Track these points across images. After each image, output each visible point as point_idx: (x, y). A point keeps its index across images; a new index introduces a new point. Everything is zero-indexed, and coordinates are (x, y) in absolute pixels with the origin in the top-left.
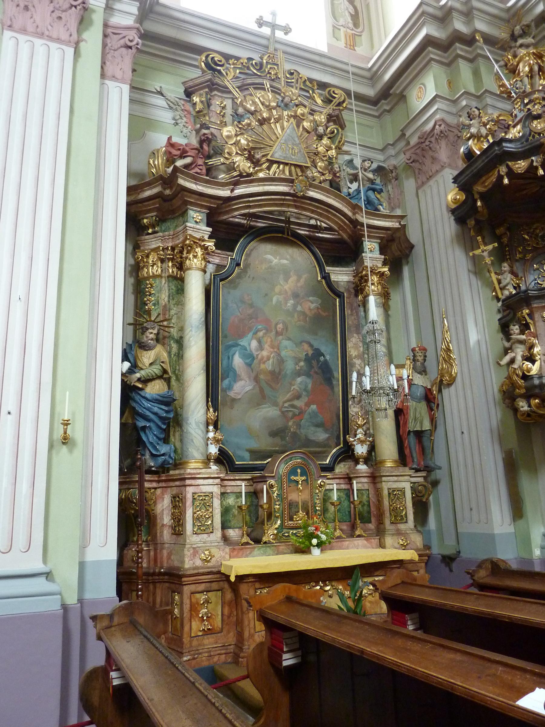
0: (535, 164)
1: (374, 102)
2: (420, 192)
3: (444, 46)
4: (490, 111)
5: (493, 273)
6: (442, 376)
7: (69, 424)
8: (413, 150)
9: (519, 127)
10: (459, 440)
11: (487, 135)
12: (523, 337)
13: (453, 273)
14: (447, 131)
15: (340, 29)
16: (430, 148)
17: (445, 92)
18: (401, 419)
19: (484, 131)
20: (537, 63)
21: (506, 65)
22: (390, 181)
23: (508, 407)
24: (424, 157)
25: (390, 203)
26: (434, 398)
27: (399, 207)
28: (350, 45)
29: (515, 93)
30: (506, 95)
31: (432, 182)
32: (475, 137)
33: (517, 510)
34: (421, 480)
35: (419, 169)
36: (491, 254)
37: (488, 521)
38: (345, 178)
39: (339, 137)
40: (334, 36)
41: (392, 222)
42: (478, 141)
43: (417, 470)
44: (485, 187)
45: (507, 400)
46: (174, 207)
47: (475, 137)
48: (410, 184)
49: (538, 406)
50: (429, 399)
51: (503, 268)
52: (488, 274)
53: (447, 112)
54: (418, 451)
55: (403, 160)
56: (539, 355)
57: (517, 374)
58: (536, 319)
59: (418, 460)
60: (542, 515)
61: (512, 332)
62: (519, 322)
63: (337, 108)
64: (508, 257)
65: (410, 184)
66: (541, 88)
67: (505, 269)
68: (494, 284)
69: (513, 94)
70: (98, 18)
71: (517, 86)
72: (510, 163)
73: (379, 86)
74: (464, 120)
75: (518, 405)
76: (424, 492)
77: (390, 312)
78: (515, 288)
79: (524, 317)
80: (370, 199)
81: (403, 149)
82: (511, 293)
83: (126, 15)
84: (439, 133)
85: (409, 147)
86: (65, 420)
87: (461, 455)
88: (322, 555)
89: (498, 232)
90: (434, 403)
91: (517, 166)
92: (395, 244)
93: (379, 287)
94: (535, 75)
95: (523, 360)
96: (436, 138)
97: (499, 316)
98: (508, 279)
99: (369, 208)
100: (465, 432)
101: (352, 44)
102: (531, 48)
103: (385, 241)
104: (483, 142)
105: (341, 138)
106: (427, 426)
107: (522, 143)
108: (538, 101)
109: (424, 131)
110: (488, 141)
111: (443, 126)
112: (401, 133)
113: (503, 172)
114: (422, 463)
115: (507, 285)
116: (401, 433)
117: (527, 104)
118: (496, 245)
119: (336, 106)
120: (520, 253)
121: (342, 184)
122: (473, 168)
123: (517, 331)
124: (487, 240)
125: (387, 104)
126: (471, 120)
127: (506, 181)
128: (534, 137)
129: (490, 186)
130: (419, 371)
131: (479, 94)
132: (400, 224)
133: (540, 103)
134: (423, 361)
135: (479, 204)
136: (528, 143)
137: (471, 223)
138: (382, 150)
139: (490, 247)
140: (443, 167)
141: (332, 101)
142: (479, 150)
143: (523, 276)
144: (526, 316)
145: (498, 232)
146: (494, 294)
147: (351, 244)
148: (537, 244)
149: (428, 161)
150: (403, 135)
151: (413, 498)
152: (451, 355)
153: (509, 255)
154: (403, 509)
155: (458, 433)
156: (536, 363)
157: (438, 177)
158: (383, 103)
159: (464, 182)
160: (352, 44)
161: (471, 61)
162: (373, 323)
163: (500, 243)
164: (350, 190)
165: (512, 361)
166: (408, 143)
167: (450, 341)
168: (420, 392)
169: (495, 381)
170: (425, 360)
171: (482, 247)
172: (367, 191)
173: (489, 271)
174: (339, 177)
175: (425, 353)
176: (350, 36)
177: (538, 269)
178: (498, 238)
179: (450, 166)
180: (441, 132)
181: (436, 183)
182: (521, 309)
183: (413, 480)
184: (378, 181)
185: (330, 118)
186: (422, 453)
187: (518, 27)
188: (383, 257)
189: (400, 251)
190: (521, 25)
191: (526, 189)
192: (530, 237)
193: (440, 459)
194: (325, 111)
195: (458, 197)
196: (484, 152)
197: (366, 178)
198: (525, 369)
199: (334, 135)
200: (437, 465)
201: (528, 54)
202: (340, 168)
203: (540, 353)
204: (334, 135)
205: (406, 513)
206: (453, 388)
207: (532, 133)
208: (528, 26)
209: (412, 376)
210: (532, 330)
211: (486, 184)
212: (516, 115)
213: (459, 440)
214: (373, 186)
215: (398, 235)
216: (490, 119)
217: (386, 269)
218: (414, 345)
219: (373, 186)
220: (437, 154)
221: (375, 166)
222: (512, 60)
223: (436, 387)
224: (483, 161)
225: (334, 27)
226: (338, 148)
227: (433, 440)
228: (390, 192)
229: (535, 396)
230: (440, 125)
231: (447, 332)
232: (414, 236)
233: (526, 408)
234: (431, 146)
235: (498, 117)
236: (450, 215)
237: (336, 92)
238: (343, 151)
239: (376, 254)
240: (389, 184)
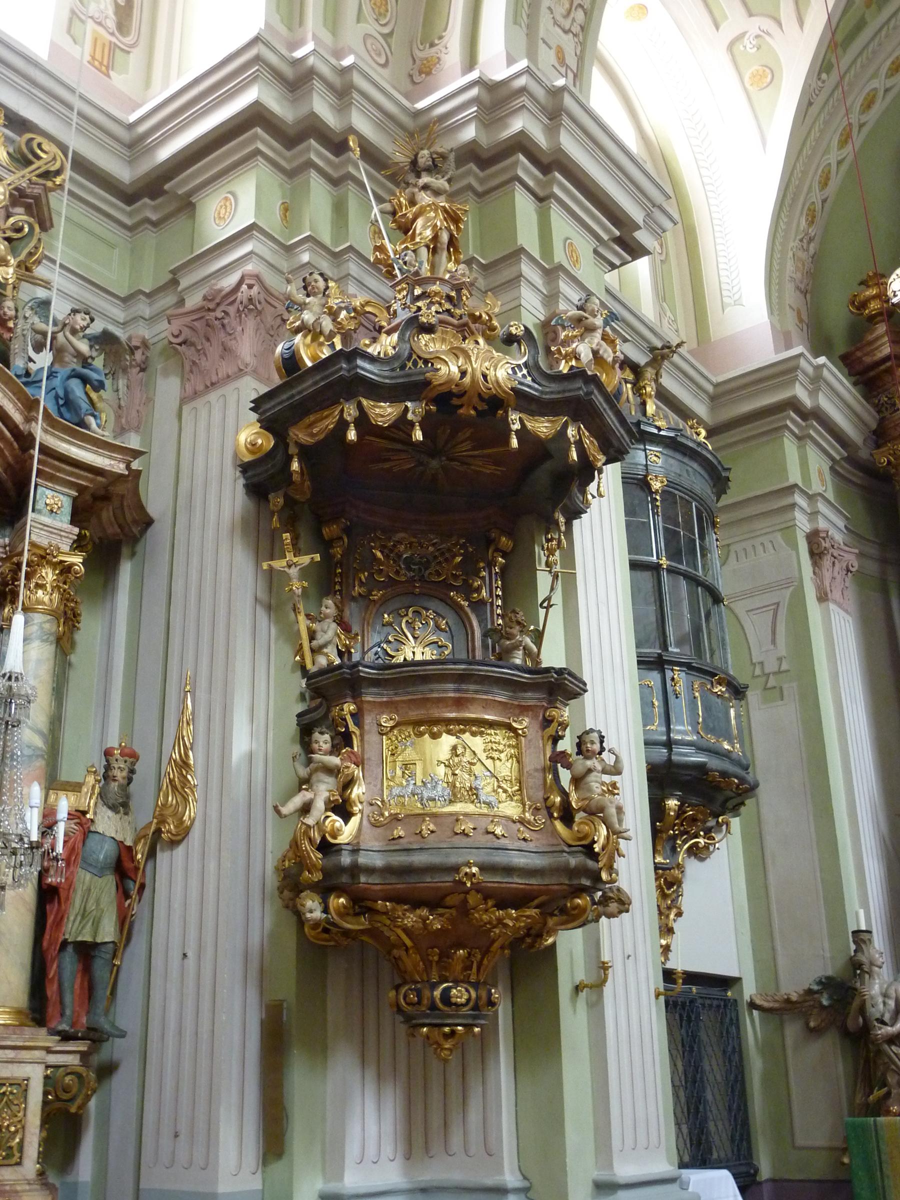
0: (410, 416)
1: (129, 196)
2: (186, 409)
3: (290, 137)
4: (352, 289)
5: (303, 614)
6: (162, 821)
8: (188, 319)
9: (395, 337)
10: (174, 974)
11: (331, 336)
12: (335, 760)
13: (222, 595)
14: (263, 301)
16: (223, 326)
17: (273, 223)
18: (52, 911)
19: (327, 324)
20: (448, 229)
21: (394, 213)
22: (125, 370)
23: (287, 907)
24: (208, 340)
25: (118, 417)
26: (137, 869)
27: (137, 429)
28: (101, 63)
29: (400, 269)
30: (384, 268)
31: (213, 396)
32: (310, 331)
33: (274, 1141)
34: (73, 1060)
35: (194, 363)
36: (305, 573)
37: (209, 1164)
38: (24, 335)
39: (32, 244)
40: (69, 31)
41: (111, 458)
42: (313, 340)
43: (66, 1037)
44: (312, 435)
45: (286, 893)
47: (310, 331)
48: (168, 388)
49: (343, 913)
50: (126, 870)
51: (323, 608)
52: (292, 615)
53: (272, 266)
54: (78, 992)
55: (163, 336)
56: (361, 803)
57: (310, 839)
58: (366, 727)
59: (73, 1012)
60: (323, 1152)
61: (315, 746)
62: (333, 726)
63: (41, 181)
64: (337, 587)
65: (168, 388)
66: (447, 276)
67: (328, 611)
68: (300, 638)
69: (397, 272)
71: (407, 258)
72: (365, 402)
73: (145, 166)
74: (295, 292)
75: (303, 905)
76: (74, 1090)
77: (73, 658)
78: (340, 654)
79: (345, 720)
80: (71, 397)
81: (169, 312)
82: (330, 663)
84: (245, 301)
85: (181, 311)
87: (173, 1007)
89: (326, 531)
90: (135, 882)
91: (378, 411)
92: (111, 508)
93: (56, 596)
94: (443, 249)
95: (326, 810)
96: (238, 310)
97: (300, 708)
98: (330, 633)
99: (67, 415)
100: (190, 954)
101: (106, 61)
102: (443, 198)
103: (87, 497)
104: (321, 344)
105: (36, 248)
106: (108, 932)
107: (393, 370)
108: (437, 299)
109: (218, 287)
110: (332, 346)
111: (256, 289)
112: (170, 276)
113: (350, 415)
114: (84, 1020)
115: (325, 645)
116: (45, 944)
117: (418, 298)
118: (317, 557)
119: (39, 176)
120: (362, 584)
121: (15, 346)
122: (294, 391)
123: (326, 747)
124: (301, 545)
125: (155, 209)
126: (308, 296)
127: (352, 435)
128: (415, 364)
129: (322, 437)
130: (111, 802)
131: (337, 250)
132: (128, 467)
133: (440, 304)
134: (125, 782)
135: (295, 466)
136: (402, 373)
137: (277, 500)
138: (126, 300)
139: (305, 560)
140: (240, 373)
141: (30, 163)
142: (313, 358)
143: (359, 632)
144: (348, 718)
145: (326, 531)
146: (298, 658)
147: (9, 485)
148: (397, 573)
149: (214, 351)
150: (174, 282)
151: (45, 1103)
152: (189, 777)
153: (341, 584)
154: (17, 1131)
155: (176, 955)
156: (353, 819)
157: (229, 390)
158: (145, 205)
159: (275, 414)
160: (106, 61)
161: (335, 182)
162: (10, 678)
163: (327, 558)
164: (31, 365)
165: (306, 809)
166: (181, 302)
167: (192, 745)
168: (104, 852)
169: (271, 847)
170: (130, 780)
171: (290, 556)
172: (70, 377)
173: (295, 609)
174: (10, 330)
175: (133, 764)
176: (104, 45)
177: (390, 624)
178: (324, 545)
179: (255, 373)
180: (250, 300)
181: (221, 400)
182: (340, 699)
183: (53, 1059)
184: (98, 363)
185: (21, 197)
186: (87, 995)
187: (425, 152)
188: (76, 530)
189: (120, 526)
190: (432, 150)
191: (389, 460)
192: (387, 557)
193: (126, 1014)
194: (10, 178)
195: (260, 441)
196: (321, 365)
197: (71, 350)
198: (328, 829)
199: (19, 235)
200: (117, 1029)
201: (435, 207)
202: (17, 311)
203: (363, 798)
204: (19, 235)
205: (22, 1141)
206: (180, 850)
207: (414, 357)
208: (443, 157)
209: (95, 813)
210: (356, 749)
211: (315, 431)
212: (395, 312)
213: (174, 974)
214: (86, 371)
215: (120, 489)
216: (343, 305)
217: (77, 560)
218: (113, 742)
219: (86, 371)
220: (233, 342)
221: (97, 328)
222: (406, 209)
223: (145, 844)
224: (316, 383)
225: (73, 12)
226: (25, 268)
227: (119, 967)
228: (121, 393)
229: (340, 890)
230: (250, 287)
231: (188, 724)
232: (156, 499)
233: (318, 914)
234: (226, 321)
235: (363, 306)
236: (238, 474)
237: (45, 147)
238: (33, 278)
239: (63, 521)
240: (121, 375)
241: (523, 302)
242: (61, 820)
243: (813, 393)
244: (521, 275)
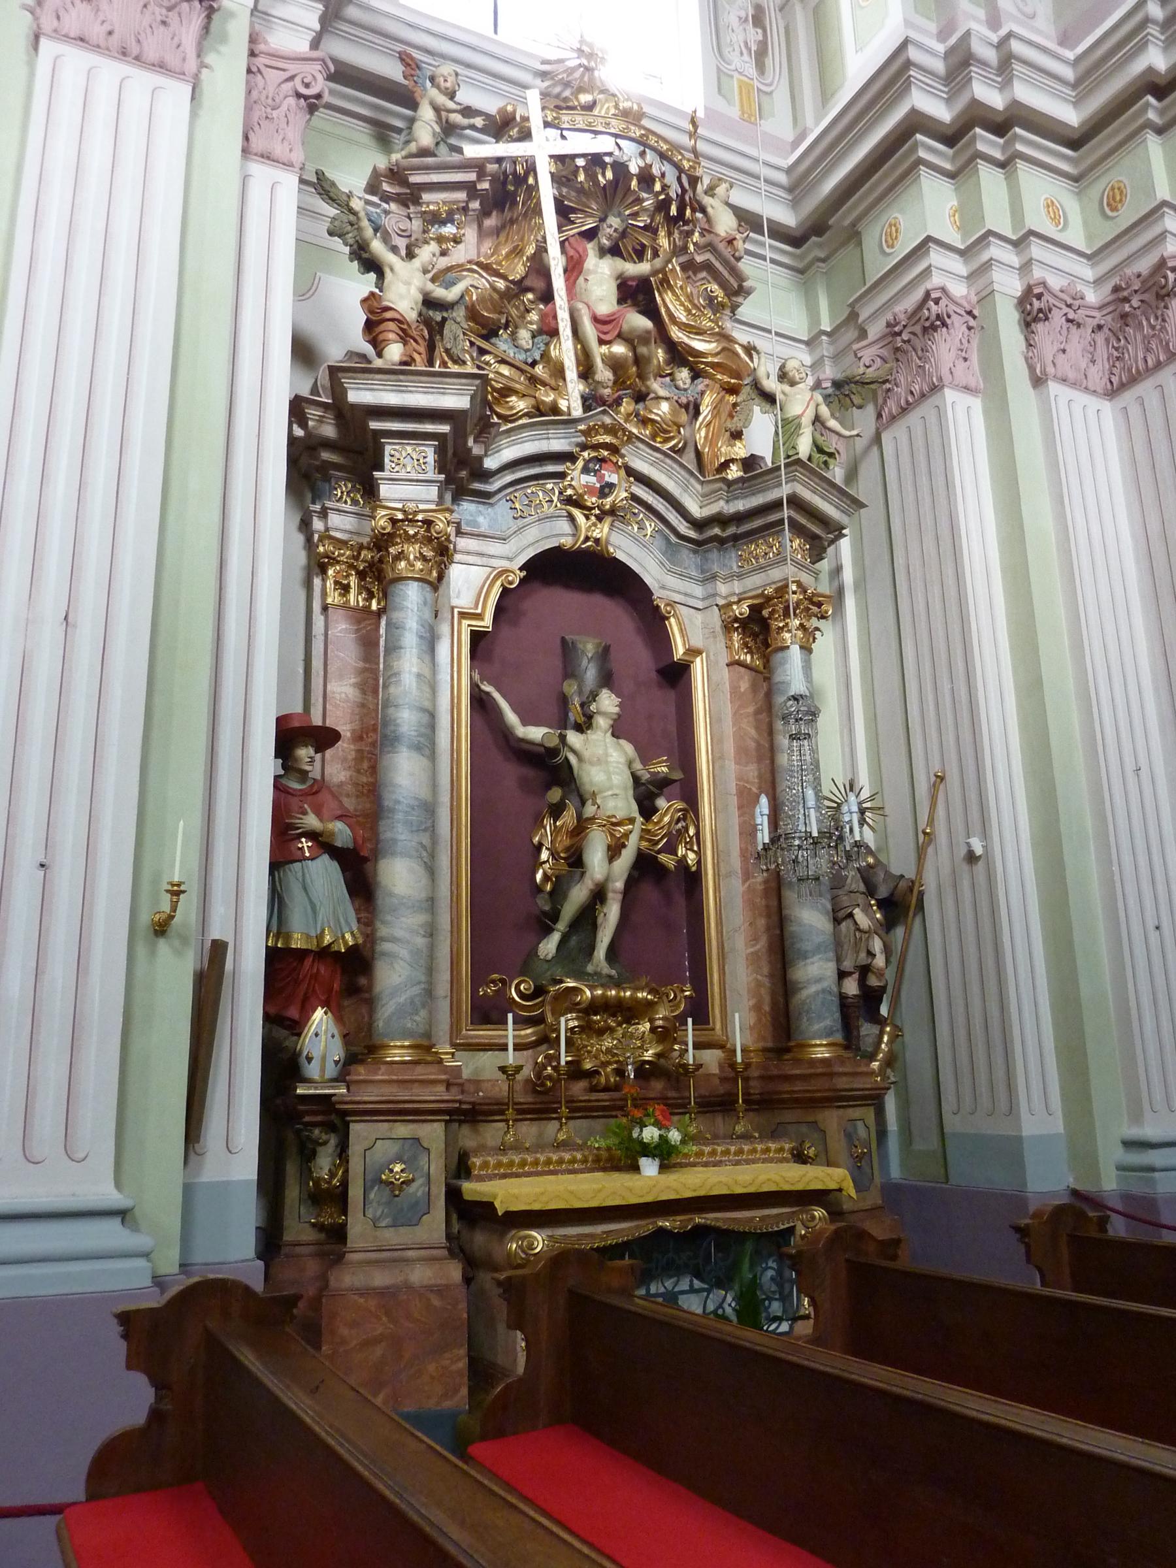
1: (795, 239)
3: (952, 137)
7: (184, 892)
15: (732, 77)
46: (792, 1044)
70: (238, 30)
83: (294, 30)
86: (173, 885)
88: (663, 1177)
150: (853, 316)
241: (996, 287)
242: (818, 949)
243: (1006, 84)
244: (1031, 259)
